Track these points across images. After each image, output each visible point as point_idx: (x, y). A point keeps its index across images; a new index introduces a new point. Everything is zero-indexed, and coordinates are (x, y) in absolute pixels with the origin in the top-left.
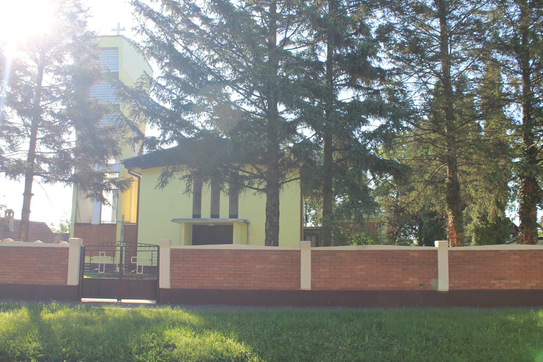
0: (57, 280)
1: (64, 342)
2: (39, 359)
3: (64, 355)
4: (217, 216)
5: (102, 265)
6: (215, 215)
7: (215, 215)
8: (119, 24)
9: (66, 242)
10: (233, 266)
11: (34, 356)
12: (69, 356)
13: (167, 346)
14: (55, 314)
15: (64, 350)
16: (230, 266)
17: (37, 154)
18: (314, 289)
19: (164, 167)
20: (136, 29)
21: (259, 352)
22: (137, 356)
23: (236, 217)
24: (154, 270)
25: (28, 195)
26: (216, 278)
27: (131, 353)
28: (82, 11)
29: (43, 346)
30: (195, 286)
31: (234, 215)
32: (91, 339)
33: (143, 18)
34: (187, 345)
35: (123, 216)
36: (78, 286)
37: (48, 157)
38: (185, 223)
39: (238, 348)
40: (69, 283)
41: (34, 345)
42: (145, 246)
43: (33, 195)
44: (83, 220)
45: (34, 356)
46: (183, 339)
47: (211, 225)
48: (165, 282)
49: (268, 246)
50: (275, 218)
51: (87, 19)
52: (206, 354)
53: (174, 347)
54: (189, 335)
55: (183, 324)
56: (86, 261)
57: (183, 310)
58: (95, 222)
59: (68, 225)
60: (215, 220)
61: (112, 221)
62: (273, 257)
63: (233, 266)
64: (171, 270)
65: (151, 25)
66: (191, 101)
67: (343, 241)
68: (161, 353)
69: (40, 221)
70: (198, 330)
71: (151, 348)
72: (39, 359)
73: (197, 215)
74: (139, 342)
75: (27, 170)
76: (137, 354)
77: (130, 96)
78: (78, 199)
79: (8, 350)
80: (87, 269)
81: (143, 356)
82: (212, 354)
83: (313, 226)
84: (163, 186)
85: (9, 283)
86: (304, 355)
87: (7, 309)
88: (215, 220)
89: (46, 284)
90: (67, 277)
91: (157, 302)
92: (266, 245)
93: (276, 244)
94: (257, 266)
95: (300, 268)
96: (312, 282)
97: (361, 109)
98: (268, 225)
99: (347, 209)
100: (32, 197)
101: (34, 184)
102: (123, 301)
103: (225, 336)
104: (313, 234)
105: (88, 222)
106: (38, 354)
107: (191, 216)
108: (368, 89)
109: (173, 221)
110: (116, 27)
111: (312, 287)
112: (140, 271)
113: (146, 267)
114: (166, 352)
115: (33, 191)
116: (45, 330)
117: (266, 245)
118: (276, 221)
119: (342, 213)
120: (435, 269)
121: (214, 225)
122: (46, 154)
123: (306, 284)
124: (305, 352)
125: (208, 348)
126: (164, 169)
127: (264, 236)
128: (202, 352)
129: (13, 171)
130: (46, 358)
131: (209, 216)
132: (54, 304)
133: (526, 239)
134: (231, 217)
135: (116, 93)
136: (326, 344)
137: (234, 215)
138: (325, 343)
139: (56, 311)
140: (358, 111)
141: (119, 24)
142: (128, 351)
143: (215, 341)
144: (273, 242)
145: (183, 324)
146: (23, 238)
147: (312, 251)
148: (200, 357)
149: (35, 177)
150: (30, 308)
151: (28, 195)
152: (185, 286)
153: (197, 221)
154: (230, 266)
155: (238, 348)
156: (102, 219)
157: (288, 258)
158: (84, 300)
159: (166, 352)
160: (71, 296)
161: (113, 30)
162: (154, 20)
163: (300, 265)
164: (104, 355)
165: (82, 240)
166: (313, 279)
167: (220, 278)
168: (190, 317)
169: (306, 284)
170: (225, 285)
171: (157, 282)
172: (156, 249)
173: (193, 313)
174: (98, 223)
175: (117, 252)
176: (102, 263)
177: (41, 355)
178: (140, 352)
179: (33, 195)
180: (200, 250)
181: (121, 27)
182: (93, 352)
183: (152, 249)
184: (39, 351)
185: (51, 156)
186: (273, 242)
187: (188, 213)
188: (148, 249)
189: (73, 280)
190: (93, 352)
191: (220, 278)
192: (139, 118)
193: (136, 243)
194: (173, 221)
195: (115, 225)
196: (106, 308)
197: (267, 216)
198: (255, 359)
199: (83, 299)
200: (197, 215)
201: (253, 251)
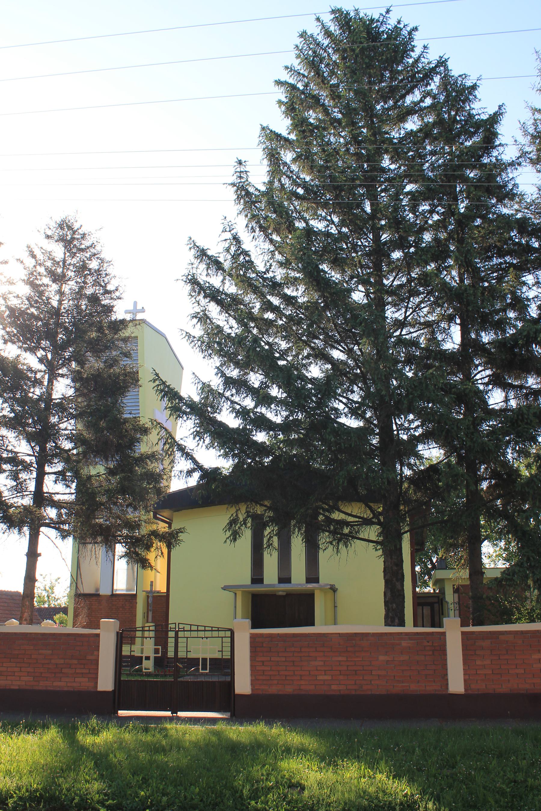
0: (81, 684)
1: (138, 781)
2: (108, 807)
3: (143, 801)
4: (288, 580)
6: (285, 579)
7: (285, 579)
8: (135, 303)
9: (50, 621)
10: (344, 659)
11: (102, 803)
12: (151, 802)
13: (292, 786)
14: (100, 737)
15: (142, 793)
16: (340, 659)
18: (470, 692)
19: (233, 510)
20: (196, 317)
21: (432, 794)
22: (253, 802)
23: (317, 580)
24: (225, 666)
25: (33, 555)
26: (320, 677)
27: (241, 797)
29: (110, 786)
30: (289, 690)
31: (313, 576)
32: (175, 775)
33: (204, 301)
34: (320, 784)
35: (152, 582)
36: (114, 691)
38: (243, 592)
39: (401, 789)
40: (100, 688)
41: (96, 786)
43: (40, 555)
44: (87, 589)
45: (102, 803)
46: (311, 774)
48: (243, 684)
49: (390, 626)
51: (115, 303)
52: (353, 798)
53: (303, 788)
54: (315, 768)
55: (302, 751)
57: (284, 728)
58: (105, 591)
59: (46, 595)
60: (285, 587)
62: (404, 644)
63: (344, 659)
64: (252, 666)
65: (214, 310)
66: (261, 413)
67: (506, 617)
68: (286, 796)
69: (13, 590)
70: (328, 759)
71: (270, 789)
72: (108, 807)
73: (257, 577)
74: (248, 779)
75: (28, 521)
76: (250, 798)
77: (188, 410)
79: (60, 793)
80: (125, 666)
81: (262, 802)
82: (363, 798)
83: (432, 591)
84: (235, 539)
85: (12, 687)
86: (502, 799)
87: (11, 727)
88: (285, 587)
89: (66, 689)
91: (231, 716)
94: (382, 658)
95: (446, 660)
96: (465, 681)
97: (531, 421)
98: (389, 594)
99: (521, 569)
100: (39, 558)
101: (42, 540)
102: (181, 714)
103: (372, 769)
105: (92, 591)
106: (107, 801)
107: (249, 582)
108: (521, 387)
110: (131, 308)
111: (466, 690)
112: (204, 668)
114: (294, 794)
116: (101, 760)
119: (513, 575)
121: (284, 594)
123: (456, 684)
124: (503, 794)
125: (353, 788)
126: (232, 515)
127: (382, 611)
128: (346, 795)
129: (13, 521)
130: (119, 806)
131: (275, 581)
132: (94, 721)
134: (309, 580)
135: (169, 408)
136: (530, 781)
137: (313, 576)
138: (529, 780)
139: (99, 731)
140: (527, 423)
141: (135, 303)
142: (238, 795)
143: (353, 776)
144: (397, 621)
145: (302, 751)
146: (26, 620)
147: (463, 633)
148: (345, 803)
149: (42, 529)
150: (62, 727)
151: (33, 555)
152: (274, 690)
153: (258, 588)
154: (340, 659)
155: (401, 789)
156: (115, 588)
157: (428, 644)
158: (122, 713)
159: (294, 794)
160: (105, 707)
161: (127, 312)
162: (219, 303)
163: (446, 655)
164: (201, 801)
166: (467, 677)
168: (304, 741)
169: (456, 684)
170: (334, 687)
171: (231, 685)
172: (228, 634)
173: (304, 731)
174: (109, 593)
175: (170, 640)
177: (110, 802)
178: (255, 795)
179: (40, 555)
181: (139, 307)
182: (185, 797)
183: (222, 634)
184: (105, 795)
185: (66, 498)
186: (397, 621)
187: (245, 576)
188: (215, 634)
189: (106, 682)
190: (185, 797)
193: (167, 624)
194: (225, 588)
195: (134, 596)
196: (168, 726)
197: (387, 582)
198: (430, 805)
199: (120, 712)
200: (257, 577)
201: (374, 634)
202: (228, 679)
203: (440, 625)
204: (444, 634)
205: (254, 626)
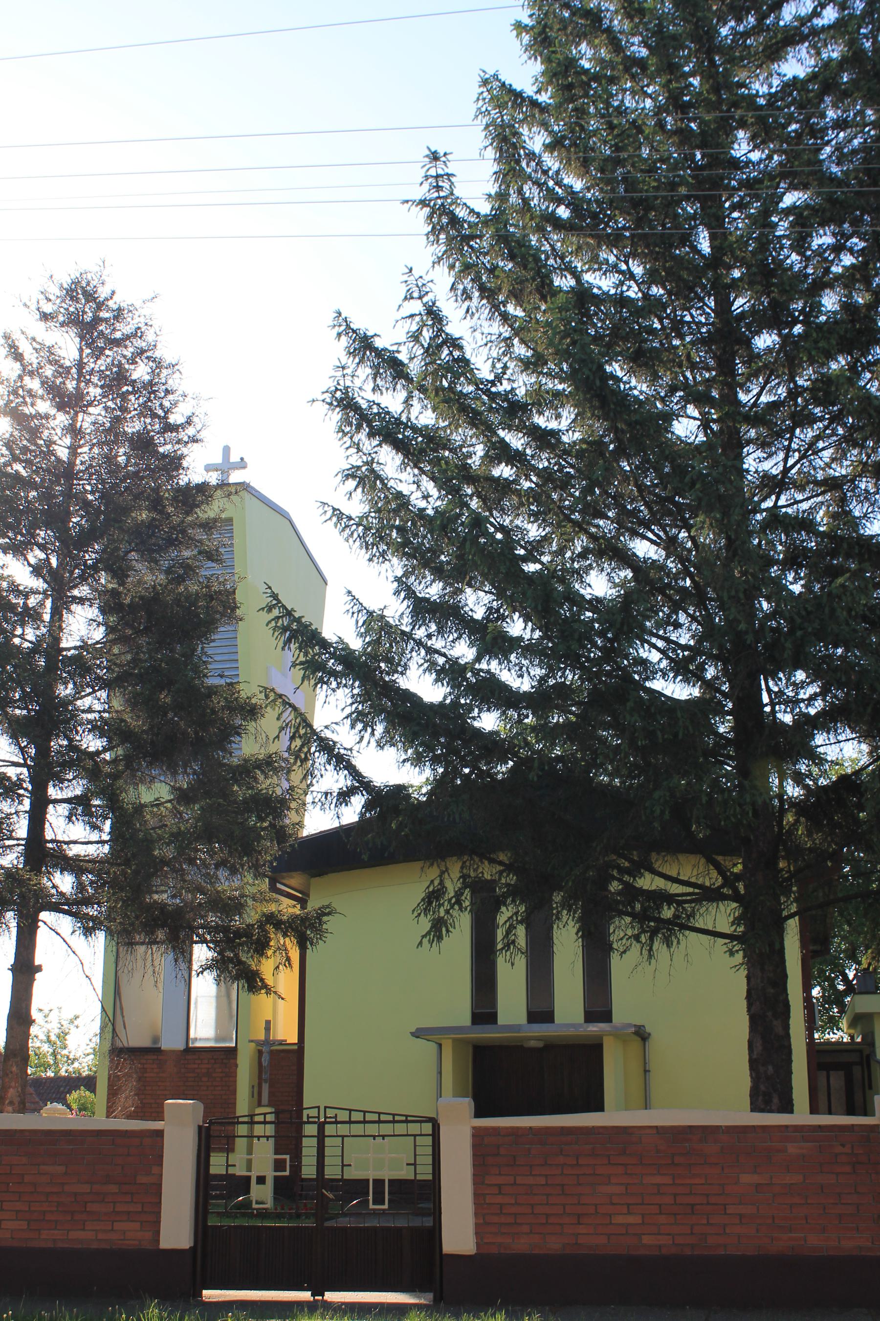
0: (128, 1234)
5: (379, 1183)
6: (541, 1013)
7: (541, 1013)
9: (60, 1106)
10: (667, 1180)
16: (658, 1180)
17: (50, 845)
23: (606, 1016)
26: (619, 1219)
28: (170, 428)
30: (554, 1245)
31: (598, 1009)
35: (268, 1023)
36: (193, 1249)
37: (71, 854)
38: (455, 1040)
42: (379, 1122)
43: (39, 969)
44: (136, 1038)
47: (533, 1044)
48: (459, 1235)
49: (762, 1111)
50: (777, 1024)
56: (213, 1171)
58: (171, 1043)
60: (541, 1030)
61: (217, 1039)
62: (793, 1149)
63: (667, 1180)
65: (389, 461)
73: (484, 1011)
78: (119, 972)
80: (216, 1197)
88: (541, 1030)
89: (94, 1246)
90: (158, 1222)
91: (436, 1300)
92: (755, 1108)
93: (866, 1110)
94: (747, 1179)
98: (759, 1046)
101: (43, 935)
102: (330, 1296)
104: (836, 1066)
105: (146, 1043)
107: (465, 1019)
109: (418, 1034)
113: (397, 1185)
115: (39, 959)
117: (755, 1108)
118: (780, 1030)
120: (155, 1170)
121: (540, 1044)
122: (65, 847)
126: (432, 882)
127: (745, 1082)
133: (35, 611)
134: (591, 1016)
135: (301, 663)
137: (598, 1009)
144: (776, 1100)
146: (11, 1103)
149: (44, 915)
153: (486, 1034)
154: (658, 1180)
158: (209, 1294)
162: (400, 446)
165: (201, 1107)
167: (631, 1219)
170: (646, 1240)
171: (434, 1234)
172: (428, 1128)
174: (181, 1046)
175: (305, 1142)
176: (379, 1175)
179: (39, 969)
180: (563, 1129)
183: (414, 1128)
186: (776, 1100)
187: (457, 1009)
188: (400, 1128)
189: (176, 1231)
191: (631, 1219)
192: (373, 734)
193: (300, 1108)
194: (418, 1034)
200: (484, 1011)
202: (428, 1222)
203: (159, 1115)
204: (160, 1133)
205: (479, 1113)
